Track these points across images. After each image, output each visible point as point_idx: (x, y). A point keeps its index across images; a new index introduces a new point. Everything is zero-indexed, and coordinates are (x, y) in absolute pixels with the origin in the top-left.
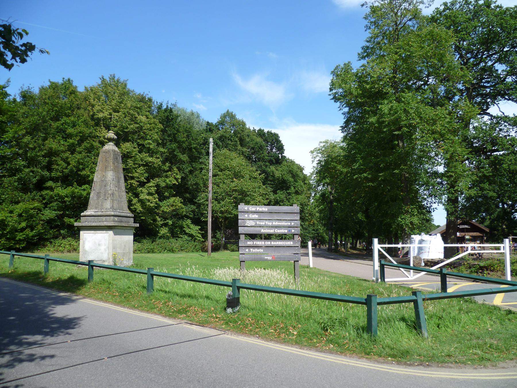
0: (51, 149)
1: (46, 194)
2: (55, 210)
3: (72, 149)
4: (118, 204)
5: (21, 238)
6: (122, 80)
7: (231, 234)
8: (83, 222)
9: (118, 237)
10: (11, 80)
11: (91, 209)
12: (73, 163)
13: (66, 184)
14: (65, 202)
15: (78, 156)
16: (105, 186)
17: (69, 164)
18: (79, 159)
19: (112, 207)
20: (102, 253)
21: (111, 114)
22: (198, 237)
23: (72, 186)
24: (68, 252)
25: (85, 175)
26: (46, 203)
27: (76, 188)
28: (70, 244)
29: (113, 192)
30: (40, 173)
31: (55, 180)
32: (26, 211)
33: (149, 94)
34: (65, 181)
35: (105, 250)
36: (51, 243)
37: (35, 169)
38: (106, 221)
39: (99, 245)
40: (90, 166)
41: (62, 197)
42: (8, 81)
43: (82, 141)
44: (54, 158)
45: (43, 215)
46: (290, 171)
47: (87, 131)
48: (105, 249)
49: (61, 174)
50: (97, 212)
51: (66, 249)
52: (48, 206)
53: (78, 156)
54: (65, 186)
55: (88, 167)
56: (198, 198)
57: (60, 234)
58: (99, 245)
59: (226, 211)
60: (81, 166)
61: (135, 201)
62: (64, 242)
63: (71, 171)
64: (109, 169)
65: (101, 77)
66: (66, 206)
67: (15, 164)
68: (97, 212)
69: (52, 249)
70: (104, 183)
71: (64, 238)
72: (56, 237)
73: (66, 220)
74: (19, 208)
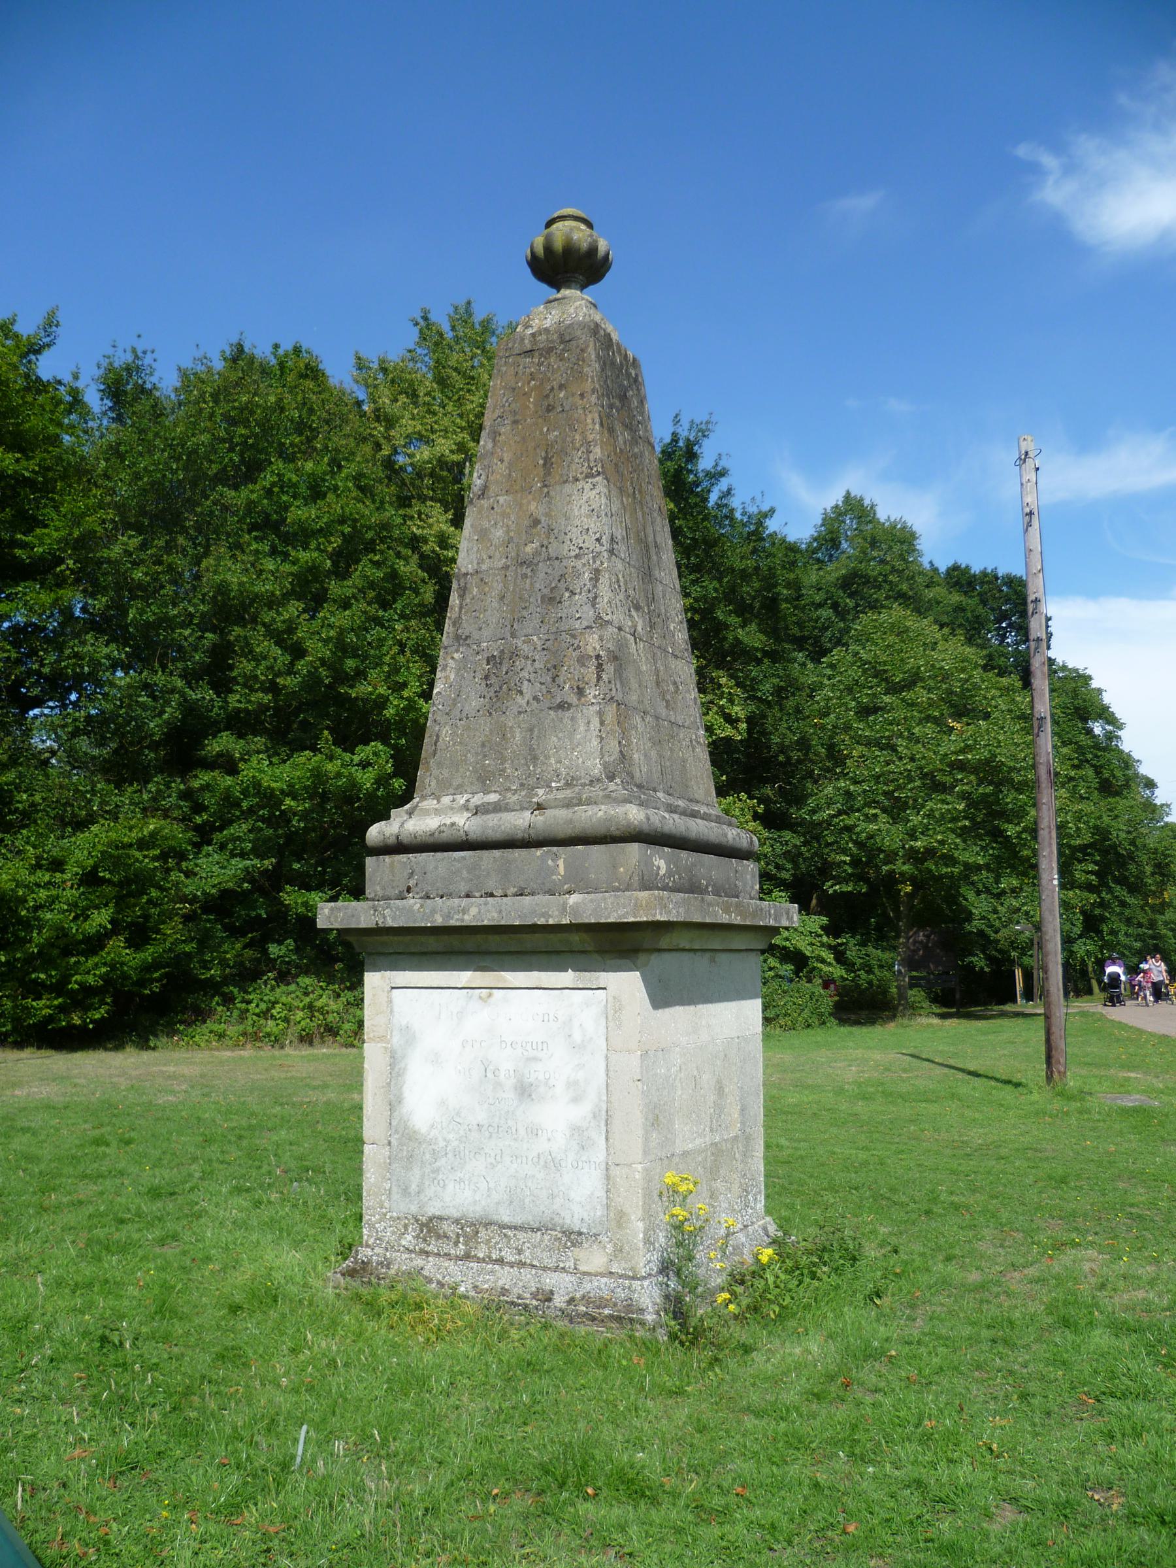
0: (222, 589)
1: (207, 787)
2: (243, 855)
3: (310, 590)
4: (657, 743)
5: (91, 980)
7: (925, 947)
8: (391, 897)
9: (680, 1019)
10: (60, 317)
11: (445, 787)
12: (317, 650)
13: (289, 743)
14: (285, 818)
15: (342, 619)
16: (552, 600)
17: (298, 652)
18: (342, 632)
19: (618, 768)
20: (552, 1164)
22: (823, 961)
23: (315, 749)
24: (302, 1039)
25: (366, 700)
26: (205, 823)
27: (331, 758)
28: (310, 1007)
29: (622, 645)
30: (183, 695)
31: (241, 724)
32: (114, 856)
34: (286, 728)
36: (228, 1000)
37: (159, 678)
38: (578, 882)
39: (525, 1091)
40: (387, 659)
41: (270, 798)
42: (50, 323)
43: (344, 561)
44: (237, 630)
45: (189, 874)
46: (1077, 709)
47: (367, 511)
49: (267, 698)
50: (497, 808)
51: (294, 1030)
52: (217, 837)
53: (342, 619)
54: (284, 750)
55: (379, 664)
56: (811, 803)
57: (271, 963)
58: (525, 1091)
59: (930, 852)
60: (350, 663)
62: (286, 994)
63: (312, 680)
64: (577, 467)
65: (418, 316)
66: (290, 838)
67: (76, 655)
68: (497, 808)
69: (232, 1030)
70: (541, 579)
71: (284, 977)
72: (247, 976)
73: (291, 897)
74: (82, 849)
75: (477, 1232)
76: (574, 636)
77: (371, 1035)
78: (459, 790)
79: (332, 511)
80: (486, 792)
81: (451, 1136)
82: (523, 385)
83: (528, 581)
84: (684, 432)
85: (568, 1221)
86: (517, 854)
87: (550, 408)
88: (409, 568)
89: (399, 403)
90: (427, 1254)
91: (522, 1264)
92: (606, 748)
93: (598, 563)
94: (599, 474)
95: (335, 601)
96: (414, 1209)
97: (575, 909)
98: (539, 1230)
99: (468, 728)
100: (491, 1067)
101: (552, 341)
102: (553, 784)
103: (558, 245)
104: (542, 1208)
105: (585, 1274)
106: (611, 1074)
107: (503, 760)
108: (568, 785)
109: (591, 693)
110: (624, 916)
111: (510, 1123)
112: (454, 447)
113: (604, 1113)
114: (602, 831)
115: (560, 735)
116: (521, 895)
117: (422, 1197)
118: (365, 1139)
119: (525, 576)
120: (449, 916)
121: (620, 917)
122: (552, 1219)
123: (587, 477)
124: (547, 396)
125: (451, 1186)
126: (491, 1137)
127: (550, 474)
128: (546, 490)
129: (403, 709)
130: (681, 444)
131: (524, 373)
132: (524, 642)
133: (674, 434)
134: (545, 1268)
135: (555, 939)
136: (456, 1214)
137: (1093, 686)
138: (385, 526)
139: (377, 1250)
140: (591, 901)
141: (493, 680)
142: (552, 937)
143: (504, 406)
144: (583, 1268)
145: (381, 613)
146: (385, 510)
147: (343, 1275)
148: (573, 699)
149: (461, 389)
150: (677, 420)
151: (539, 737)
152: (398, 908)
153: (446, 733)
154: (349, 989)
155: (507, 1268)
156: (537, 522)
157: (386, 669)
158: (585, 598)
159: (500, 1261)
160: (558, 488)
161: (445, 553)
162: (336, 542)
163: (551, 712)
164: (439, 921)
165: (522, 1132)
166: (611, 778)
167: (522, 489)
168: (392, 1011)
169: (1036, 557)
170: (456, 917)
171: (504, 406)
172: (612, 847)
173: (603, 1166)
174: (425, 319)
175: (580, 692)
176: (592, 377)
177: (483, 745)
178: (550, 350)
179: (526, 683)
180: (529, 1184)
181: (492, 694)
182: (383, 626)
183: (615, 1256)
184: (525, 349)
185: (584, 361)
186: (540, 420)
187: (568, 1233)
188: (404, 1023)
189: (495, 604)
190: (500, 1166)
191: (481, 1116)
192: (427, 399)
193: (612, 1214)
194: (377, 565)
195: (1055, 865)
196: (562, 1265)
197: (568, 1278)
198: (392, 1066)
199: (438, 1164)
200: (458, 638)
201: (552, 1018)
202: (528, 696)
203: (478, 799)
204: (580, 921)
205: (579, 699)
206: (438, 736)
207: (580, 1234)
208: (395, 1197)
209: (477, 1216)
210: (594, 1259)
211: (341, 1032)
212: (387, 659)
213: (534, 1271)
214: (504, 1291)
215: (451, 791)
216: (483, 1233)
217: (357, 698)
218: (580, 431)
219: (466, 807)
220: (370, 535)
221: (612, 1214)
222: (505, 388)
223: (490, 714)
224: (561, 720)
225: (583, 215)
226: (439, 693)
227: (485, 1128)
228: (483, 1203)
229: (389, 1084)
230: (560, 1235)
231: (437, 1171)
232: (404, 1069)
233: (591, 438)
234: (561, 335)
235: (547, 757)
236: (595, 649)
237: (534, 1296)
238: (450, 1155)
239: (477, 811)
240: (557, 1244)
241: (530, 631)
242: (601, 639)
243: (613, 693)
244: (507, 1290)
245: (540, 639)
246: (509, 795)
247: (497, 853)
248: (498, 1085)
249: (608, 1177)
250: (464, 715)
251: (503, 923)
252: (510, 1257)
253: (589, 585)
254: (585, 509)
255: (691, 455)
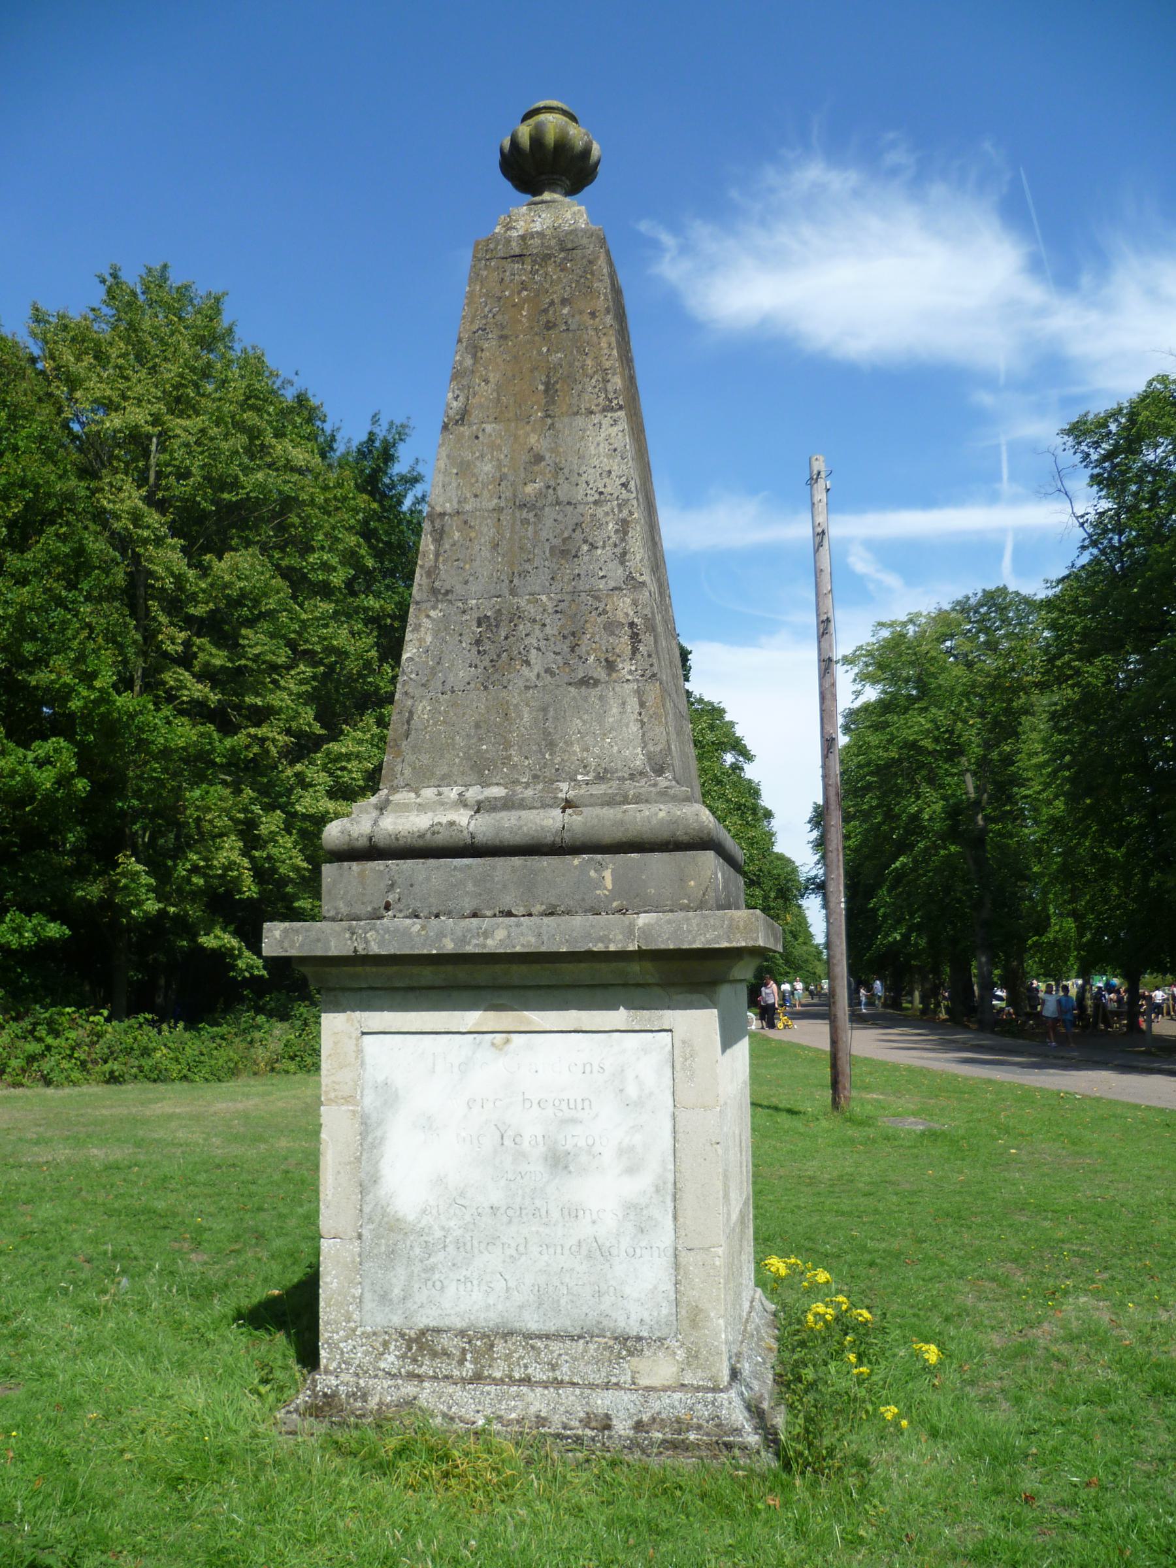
6: (200, 290)
11: (421, 777)
16: (565, 552)
18: (24, 609)
20: (600, 1253)
21: (156, 420)
33: (295, 379)
35: (637, 1216)
39: (559, 1161)
40: (75, 644)
48: (632, 1208)
50: (507, 804)
55: (63, 649)
58: (559, 1161)
61: (271, 822)
64: (591, 397)
75: (492, 1346)
76: (597, 598)
77: (332, 1095)
78: (446, 780)
79: (12, 471)
80: (485, 784)
81: (452, 1224)
82: (512, 295)
83: (531, 528)
84: (381, 432)
85: (622, 1324)
86: (545, 862)
87: (549, 326)
88: (97, 545)
89: (85, 364)
90: (419, 1378)
91: (558, 1383)
92: (650, 734)
93: (625, 512)
94: (621, 408)
95: (13, 575)
96: (397, 1320)
97: (646, 932)
98: (580, 1337)
99: (455, 704)
100: (510, 1133)
101: (549, 247)
102: (579, 777)
103: (550, 137)
104: (585, 1309)
105: (648, 1389)
106: (680, 1136)
107: (507, 746)
108: (600, 778)
109: (626, 668)
110: (715, 940)
111: (538, 1203)
112: (149, 418)
113: (670, 1186)
114: (665, 835)
115: (585, 717)
116: (552, 914)
117: (409, 1304)
118: (323, 1231)
119: (525, 522)
120: (464, 941)
121: (708, 942)
122: (599, 1322)
123: (604, 410)
124: (545, 311)
125: (451, 1289)
126: (510, 1222)
127: (554, 402)
128: (549, 421)
129: (92, 702)
130: (377, 444)
131: (512, 281)
132: (529, 601)
133: (371, 433)
134: (592, 1386)
135: (605, 970)
136: (460, 1324)
137: (727, 719)
138: (69, 497)
139: (345, 1377)
140: (669, 922)
141: (487, 646)
142: (603, 966)
143: (486, 317)
144: (643, 1382)
145: (64, 593)
146: (69, 479)
147: (302, 1415)
148: (601, 673)
149: (157, 356)
150: (375, 419)
151: (556, 719)
152: (387, 931)
153: (423, 710)
154: (15, 1019)
155: (539, 1390)
156: (539, 458)
157: (72, 655)
158: (610, 554)
159: (527, 1381)
160: (566, 420)
161: (140, 532)
162: (16, 508)
163: (572, 689)
164: (449, 946)
165: (555, 1214)
166: (660, 771)
167: (517, 419)
168: (363, 1064)
169: (826, 577)
170: (475, 941)
171: (486, 317)
172: (679, 855)
173: (671, 1251)
174: (114, 276)
175: (610, 666)
176: (605, 294)
177: (477, 726)
178: (547, 257)
179: (534, 651)
180: (567, 1280)
181: (487, 663)
182: (66, 608)
183: (689, 1364)
184: (512, 253)
185: (592, 274)
186: (537, 338)
187: (623, 1339)
188: (380, 1078)
189: (486, 553)
190: (524, 1258)
191: (496, 1196)
192: (121, 361)
193: (683, 1312)
194: (63, 538)
195: (842, 888)
196: (614, 1380)
197: (627, 1397)
198: (364, 1135)
199: (431, 1260)
200: (434, 591)
201: (596, 1068)
202: (537, 668)
203: (474, 793)
204: (653, 947)
205: (609, 675)
206: (411, 713)
207: (639, 1339)
208: (369, 1305)
209: (491, 1324)
210: (659, 1369)
211: (8, 1070)
212: (75, 644)
213: (578, 1392)
214: (541, 1421)
215: (434, 782)
216: (500, 1347)
217: (37, 687)
218: (592, 355)
219: (462, 802)
220: (52, 504)
221: (683, 1312)
222: (487, 295)
223: (486, 688)
224: (586, 699)
225: (565, 107)
226: (410, 659)
227: (502, 1211)
228: (500, 1307)
229: (358, 1159)
230: (611, 1343)
231: (432, 1269)
232: (382, 1138)
233: (607, 365)
234: (561, 242)
235: (569, 744)
236: (627, 614)
237: (586, 1422)
238: (451, 1248)
239: (479, 808)
240: (606, 1353)
241: (537, 589)
242: (635, 603)
243: (655, 669)
244: (545, 1419)
245: (550, 599)
246: (519, 789)
247: (516, 861)
248: (520, 1156)
249: (677, 1266)
250: (448, 687)
251: (543, 949)
252: (538, 1373)
253: (615, 538)
254: (604, 448)
255: (387, 456)
